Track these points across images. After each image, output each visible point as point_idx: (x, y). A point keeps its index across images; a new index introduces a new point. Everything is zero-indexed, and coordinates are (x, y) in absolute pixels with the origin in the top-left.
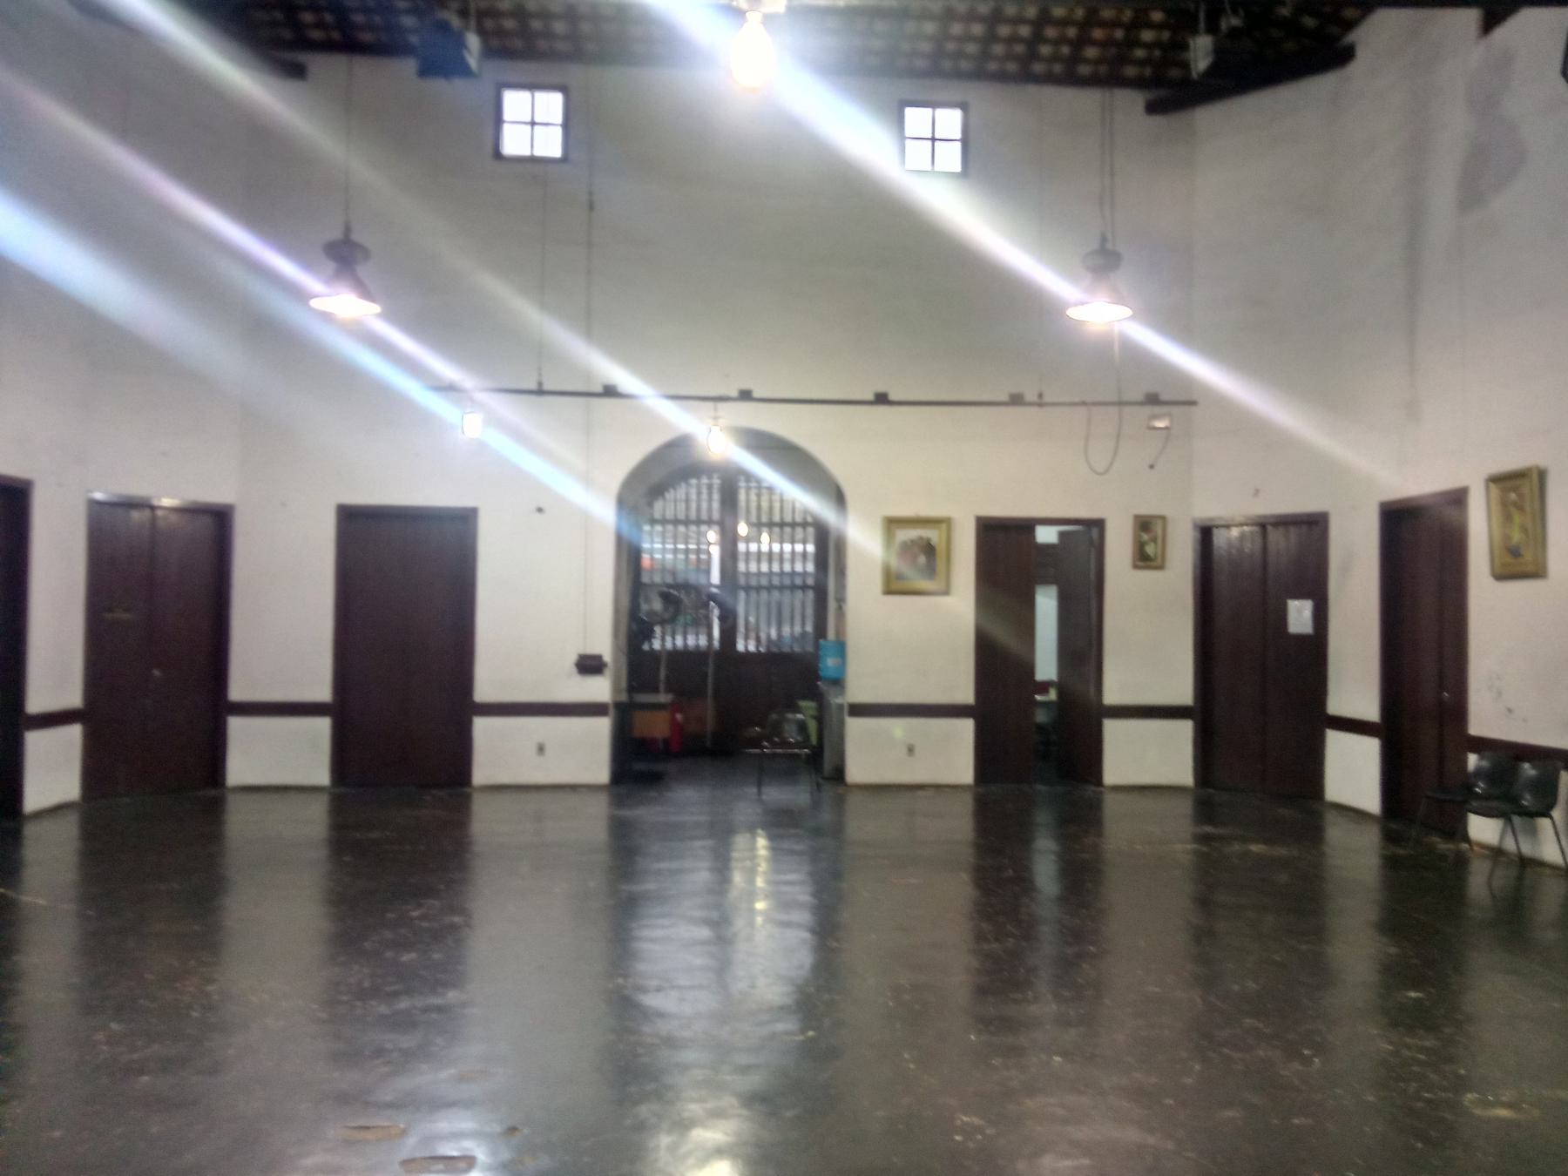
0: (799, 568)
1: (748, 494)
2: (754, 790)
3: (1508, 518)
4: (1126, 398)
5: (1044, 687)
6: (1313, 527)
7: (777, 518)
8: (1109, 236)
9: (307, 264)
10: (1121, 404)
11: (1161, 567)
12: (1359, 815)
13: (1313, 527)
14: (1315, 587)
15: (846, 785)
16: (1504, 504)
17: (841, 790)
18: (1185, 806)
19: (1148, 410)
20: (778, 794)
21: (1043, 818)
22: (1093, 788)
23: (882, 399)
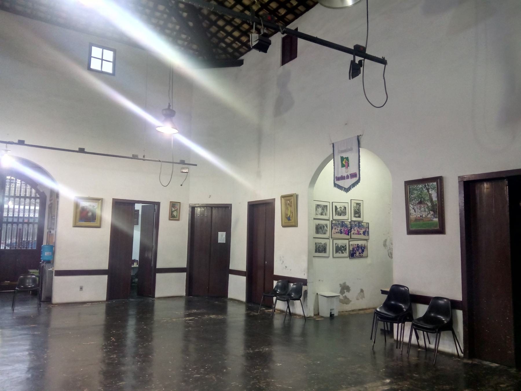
0: (32, 215)
1: (10, 185)
2: (10, 308)
3: (287, 209)
4: (175, 161)
5: (134, 261)
6: (226, 209)
7: (18, 194)
8: (171, 104)
9: (156, 117)
10: (173, 163)
11: (178, 220)
12: (239, 302)
13: (226, 209)
14: (227, 227)
15: (52, 304)
16: (286, 204)
17: (50, 306)
18: (182, 303)
19: (181, 166)
20: (21, 310)
21: (132, 312)
22: (151, 299)
23: (82, 151)
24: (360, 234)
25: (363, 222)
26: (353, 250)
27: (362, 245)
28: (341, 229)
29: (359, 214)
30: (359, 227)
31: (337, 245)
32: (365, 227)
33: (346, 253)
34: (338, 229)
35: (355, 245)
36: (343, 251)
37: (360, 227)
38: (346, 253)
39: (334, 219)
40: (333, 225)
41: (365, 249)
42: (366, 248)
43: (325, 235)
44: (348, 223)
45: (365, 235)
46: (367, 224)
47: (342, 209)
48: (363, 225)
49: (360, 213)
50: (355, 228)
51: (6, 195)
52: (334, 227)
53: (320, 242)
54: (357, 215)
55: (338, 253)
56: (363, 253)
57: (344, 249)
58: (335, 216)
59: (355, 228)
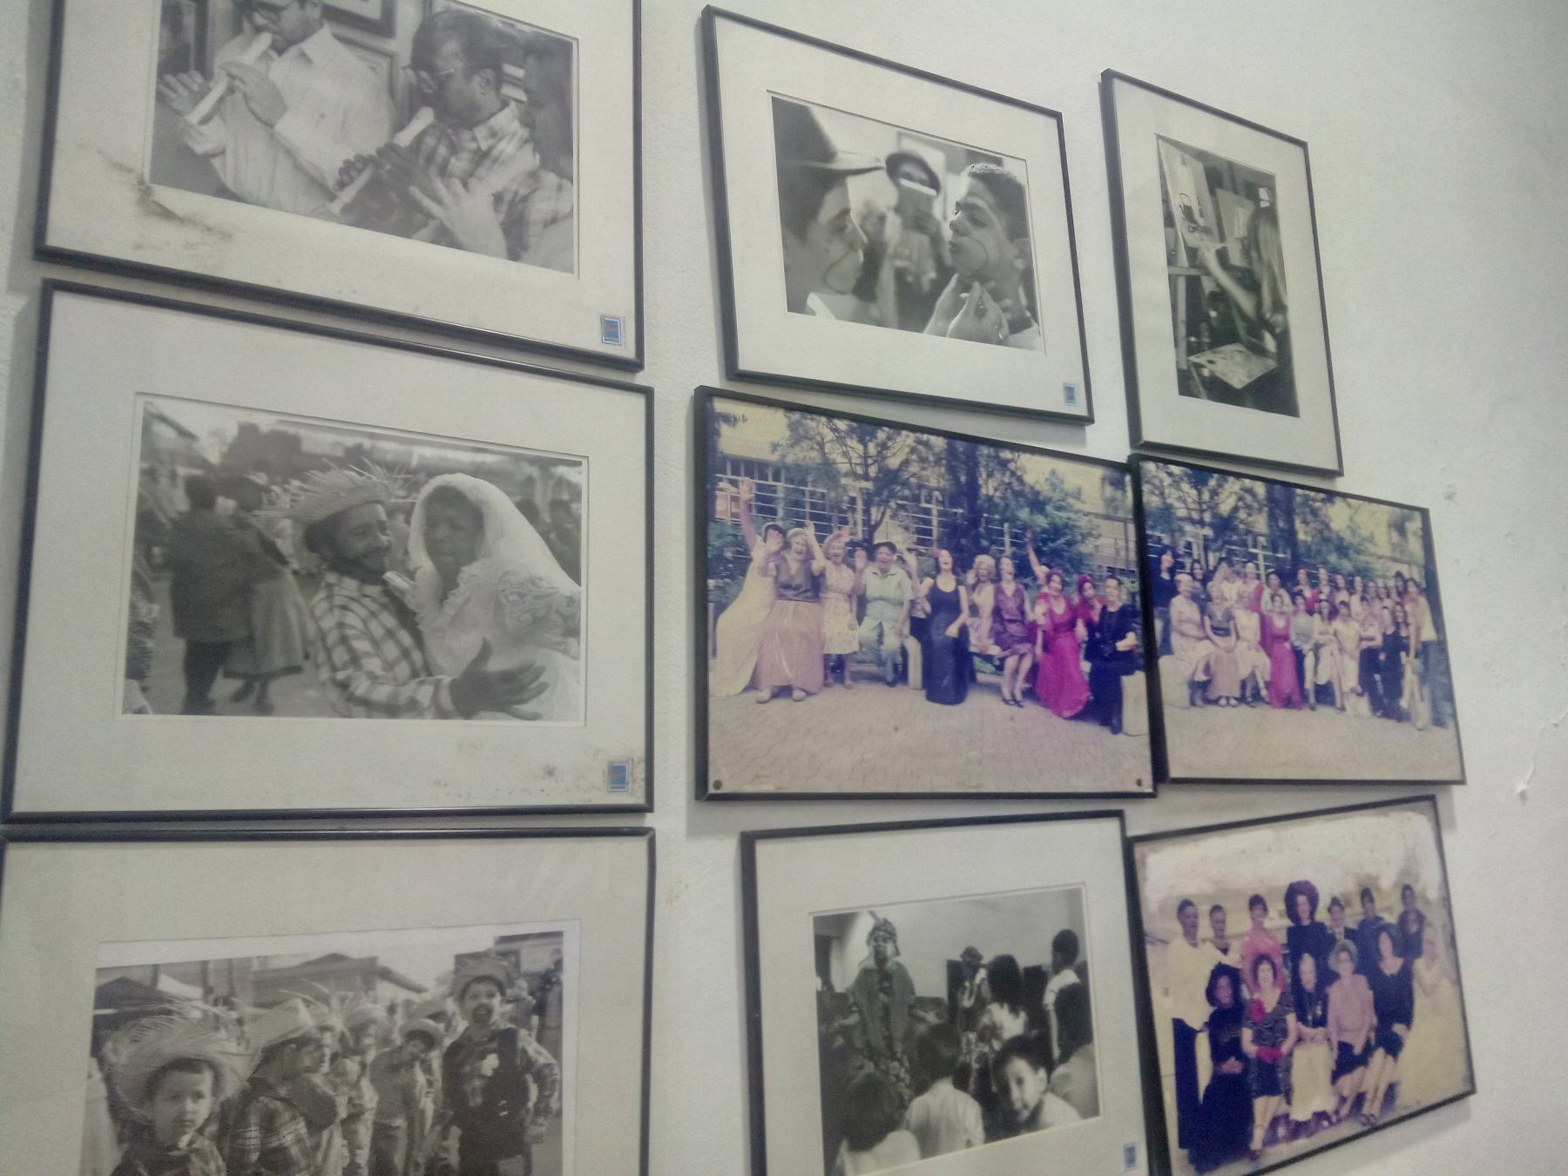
24: (1325, 694)
25: (1340, 485)
26: (1225, 1019)
27: (1366, 895)
28: (945, 605)
29: (1260, 351)
30: (1287, 578)
31: (856, 954)
32: (1386, 571)
33: (1090, 1108)
34: (873, 583)
35: (1257, 902)
36: (1027, 1082)
37: (1314, 581)
38: (1090, 1108)
39: (747, 363)
40: (731, 497)
41: (1420, 965)
42: (1433, 935)
43: (489, 729)
44: (1088, 486)
45: (1399, 716)
46: (1400, 528)
47: (945, 211)
48: (1343, 550)
49: (1283, 339)
50: (1227, 589)
51: (880, 556)
52: (762, 549)
53: (290, 950)
54: (1235, 367)
55: (901, 1141)
56: (1393, 1046)
57: (1037, 1018)
58: (796, 304)
59: (1227, 589)
